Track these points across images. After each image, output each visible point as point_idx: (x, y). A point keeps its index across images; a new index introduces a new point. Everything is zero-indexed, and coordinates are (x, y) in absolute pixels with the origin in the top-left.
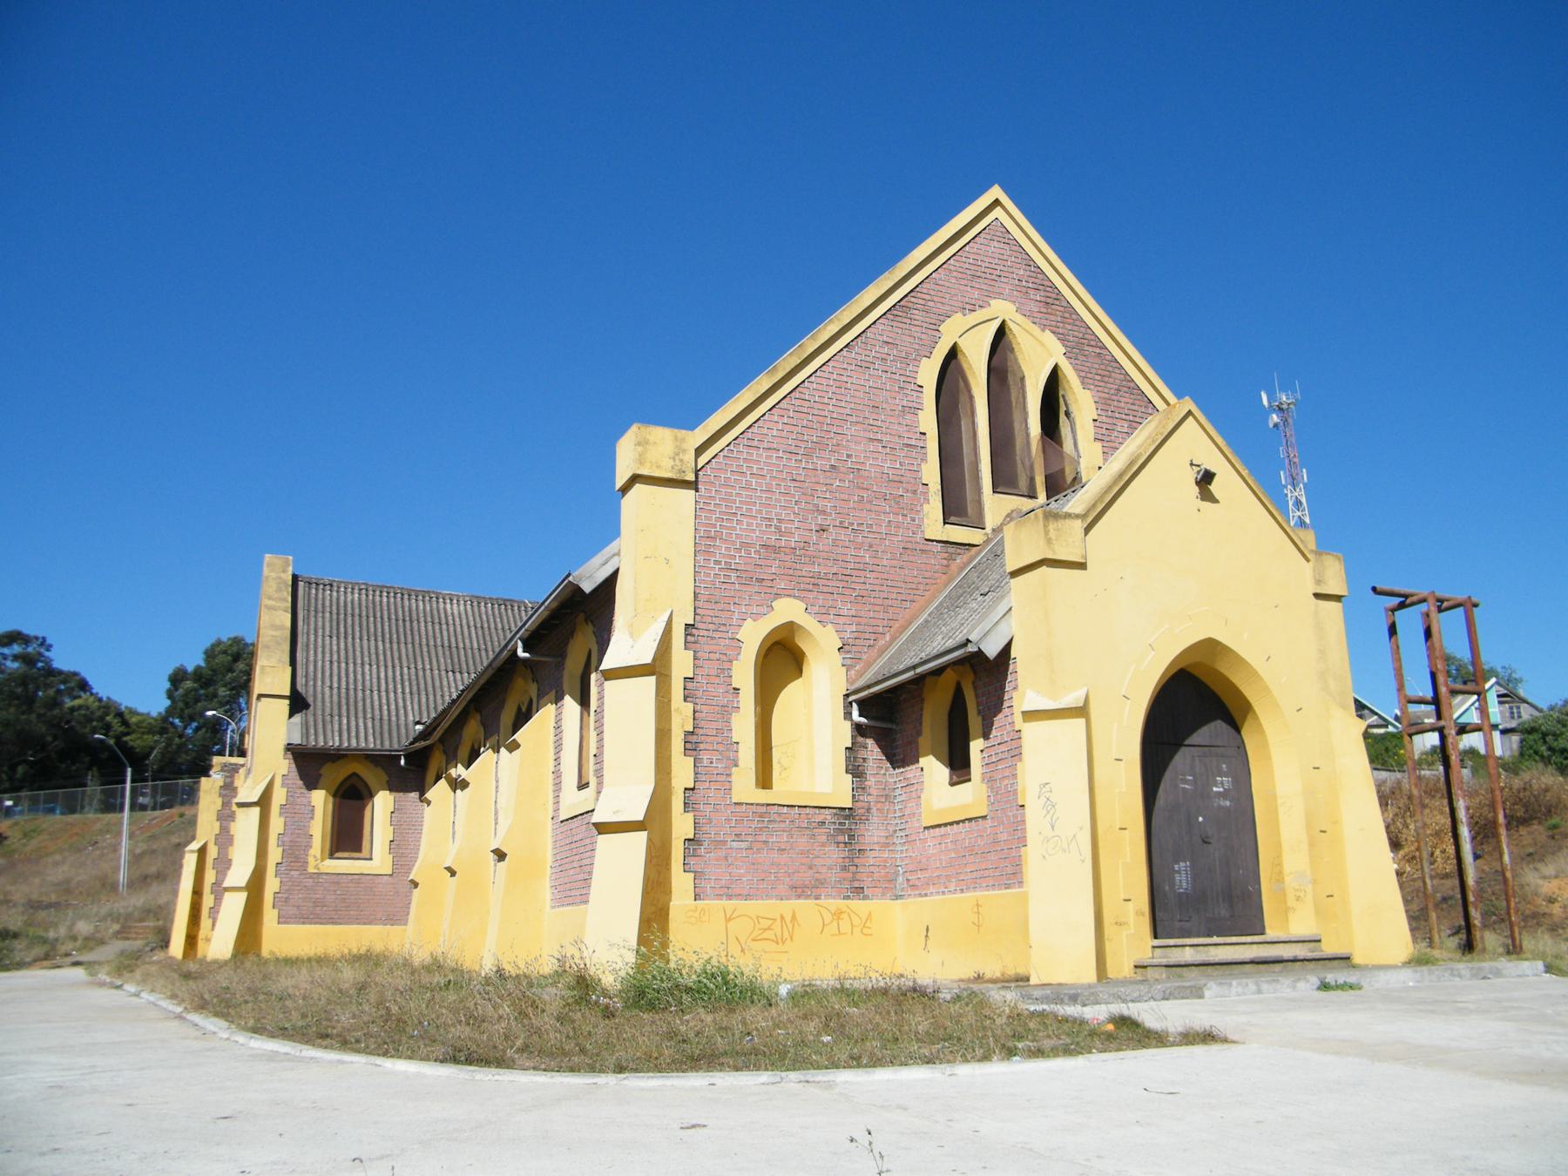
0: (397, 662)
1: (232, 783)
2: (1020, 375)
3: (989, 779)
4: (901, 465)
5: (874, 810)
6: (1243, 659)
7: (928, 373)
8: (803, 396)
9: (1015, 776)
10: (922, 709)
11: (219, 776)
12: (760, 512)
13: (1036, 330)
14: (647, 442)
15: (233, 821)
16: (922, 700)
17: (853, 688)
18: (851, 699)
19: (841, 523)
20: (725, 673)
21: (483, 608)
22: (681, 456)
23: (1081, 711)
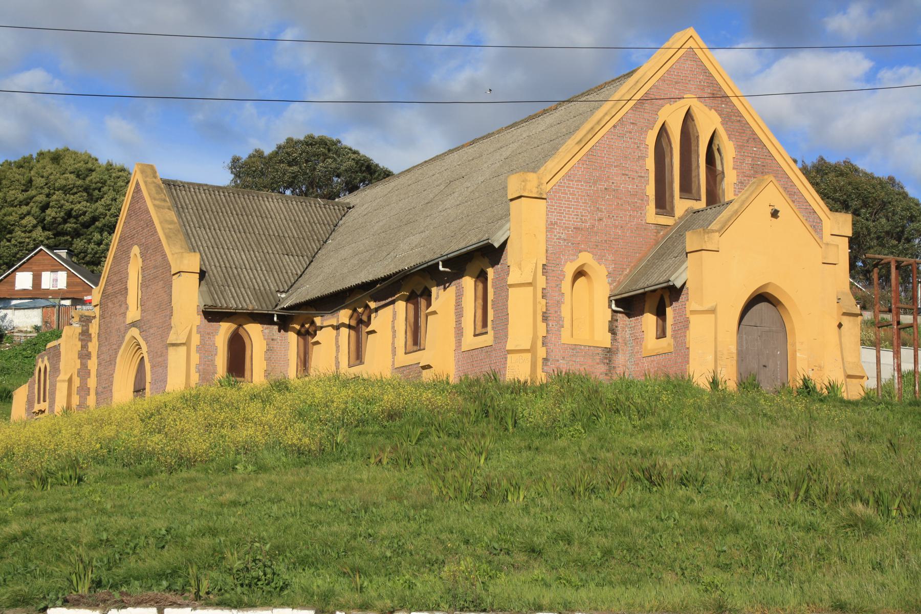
0: (249, 247)
1: (88, 330)
2: (696, 134)
3: (674, 337)
4: (637, 186)
5: (620, 349)
6: (785, 292)
7: (651, 138)
8: (593, 154)
9: (685, 336)
10: (644, 305)
11: (77, 325)
12: (573, 212)
13: (706, 109)
14: (526, 180)
15: (90, 359)
16: (645, 301)
17: (613, 294)
18: (612, 298)
19: (609, 216)
20: (559, 286)
21: (290, 205)
22: (541, 187)
23: (713, 311)
